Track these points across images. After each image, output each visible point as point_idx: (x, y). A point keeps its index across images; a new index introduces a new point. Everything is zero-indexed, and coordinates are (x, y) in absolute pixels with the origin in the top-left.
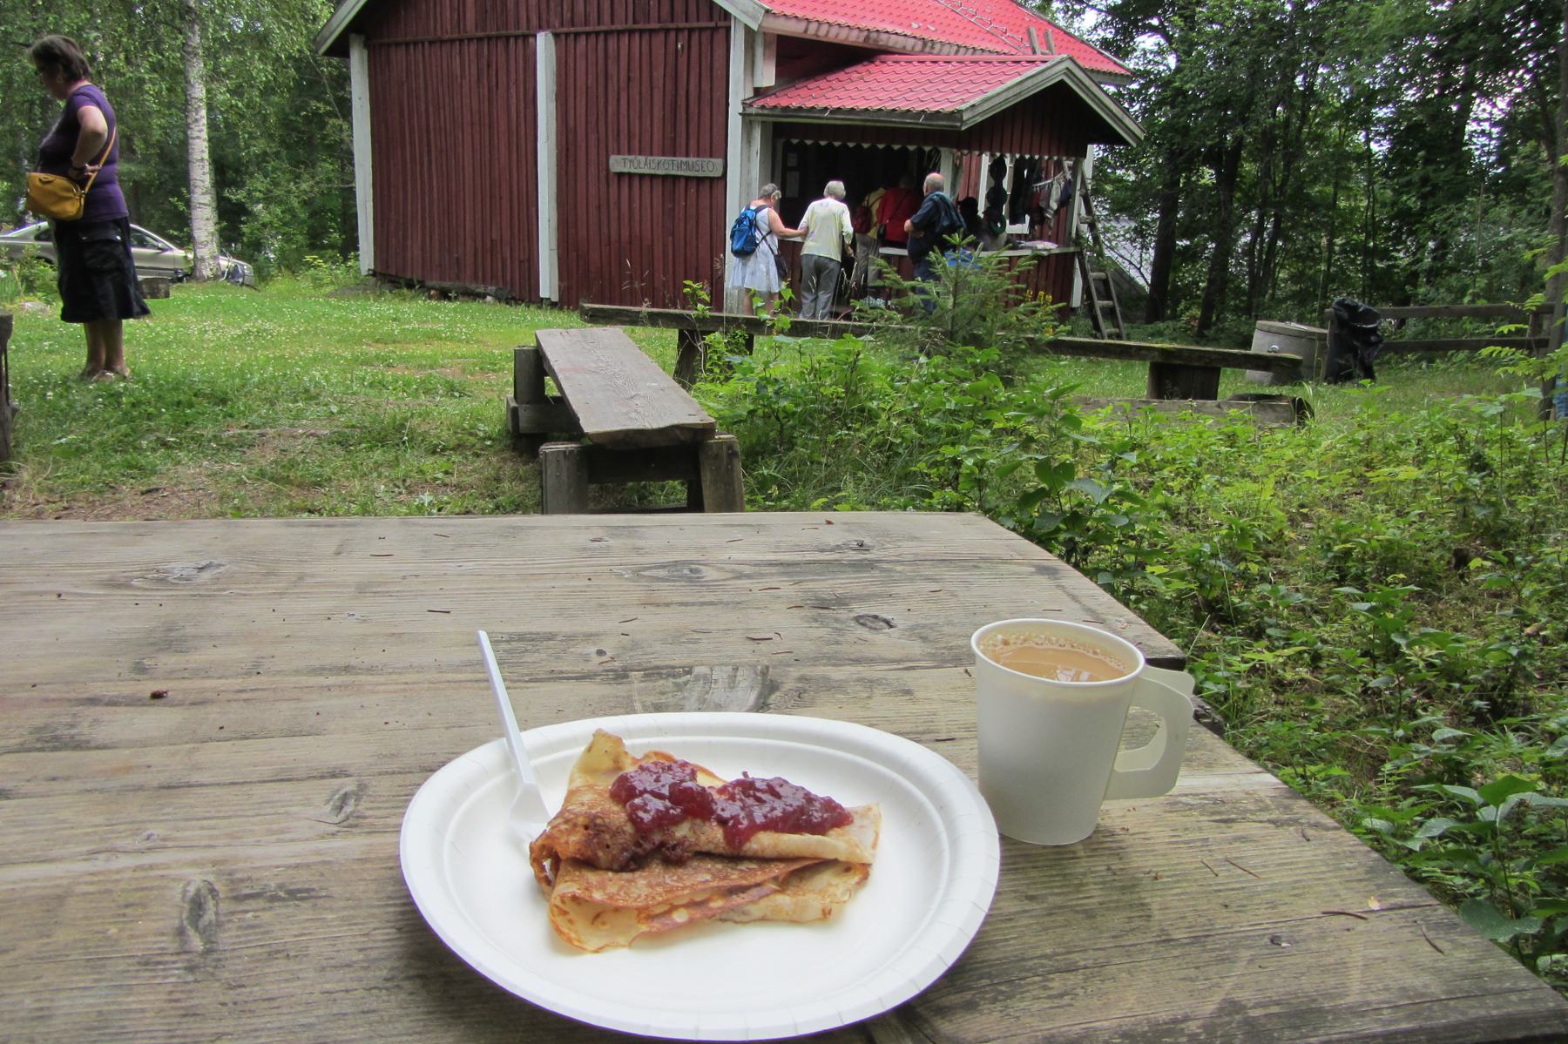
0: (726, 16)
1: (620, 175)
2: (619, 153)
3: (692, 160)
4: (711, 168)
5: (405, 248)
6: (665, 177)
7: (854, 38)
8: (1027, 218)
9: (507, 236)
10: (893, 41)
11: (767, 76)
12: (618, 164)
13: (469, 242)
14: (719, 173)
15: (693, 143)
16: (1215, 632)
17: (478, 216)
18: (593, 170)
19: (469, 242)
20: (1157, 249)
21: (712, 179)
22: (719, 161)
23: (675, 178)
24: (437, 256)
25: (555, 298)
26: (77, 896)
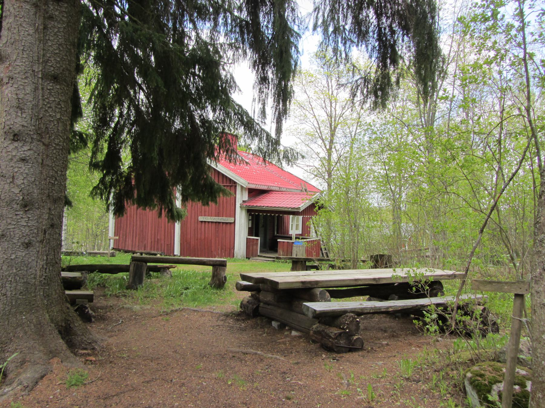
0: (235, 183)
1: (202, 222)
2: (201, 216)
3: (224, 218)
4: (231, 220)
5: (125, 241)
6: (216, 222)
7: (265, 188)
8: (173, 131)
9: (163, 237)
10: (273, 188)
11: (246, 197)
12: (201, 219)
13: (149, 239)
14: (233, 221)
15: (224, 214)
16: (239, 371)
17: (153, 232)
18: (193, 220)
19: (149, 239)
20: (120, 40)
21: (230, 223)
22: (233, 219)
23: (219, 223)
24: (137, 243)
25: (179, 255)
26: (469, 266)
